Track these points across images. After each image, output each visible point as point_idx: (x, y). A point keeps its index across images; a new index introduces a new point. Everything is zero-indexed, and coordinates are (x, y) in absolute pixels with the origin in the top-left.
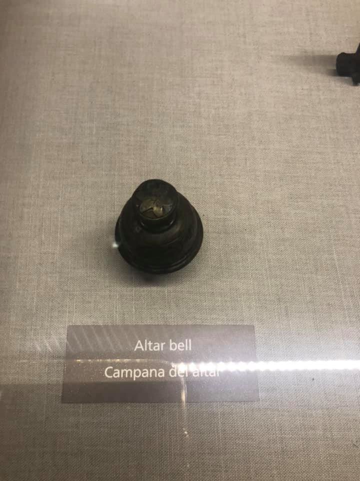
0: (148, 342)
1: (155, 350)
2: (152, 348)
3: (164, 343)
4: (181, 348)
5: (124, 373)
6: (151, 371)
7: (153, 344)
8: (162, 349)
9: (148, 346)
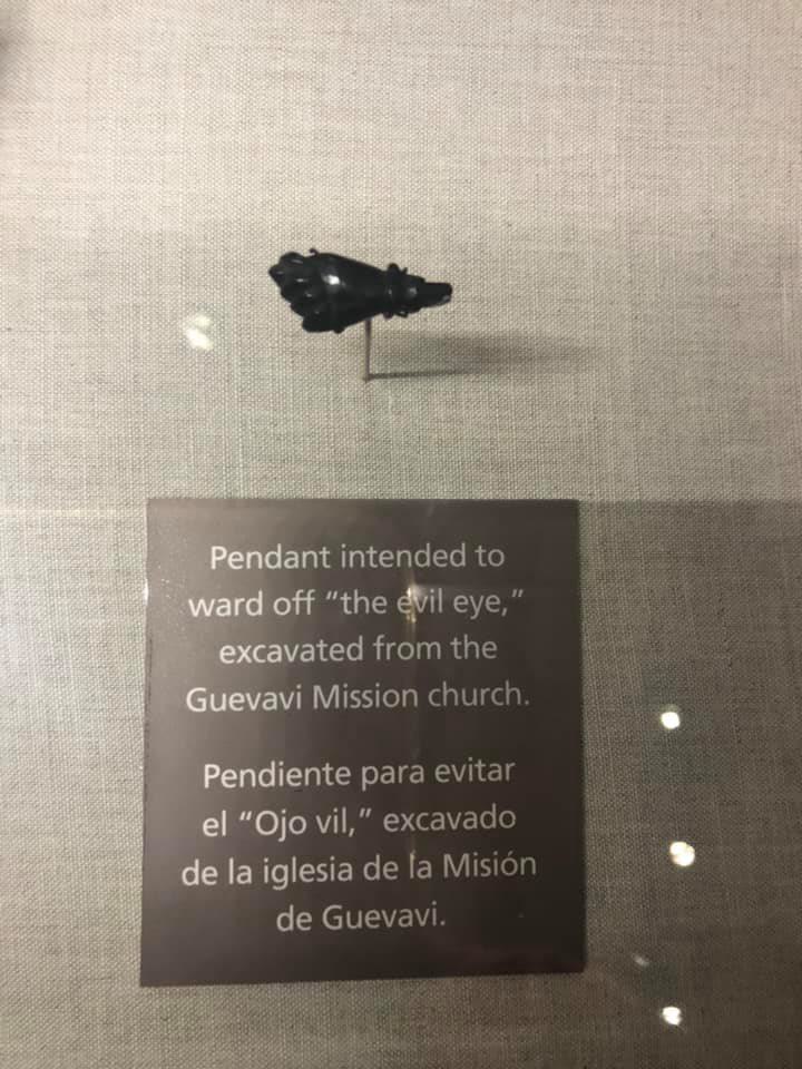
0: (475, 761)
1: (491, 779)
2: (484, 775)
3: (513, 764)
4: (293, 780)
5: (424, 649)
6: (305, 555)
7: (487, 766)
8: (508, 778)
9: (475, 770)
